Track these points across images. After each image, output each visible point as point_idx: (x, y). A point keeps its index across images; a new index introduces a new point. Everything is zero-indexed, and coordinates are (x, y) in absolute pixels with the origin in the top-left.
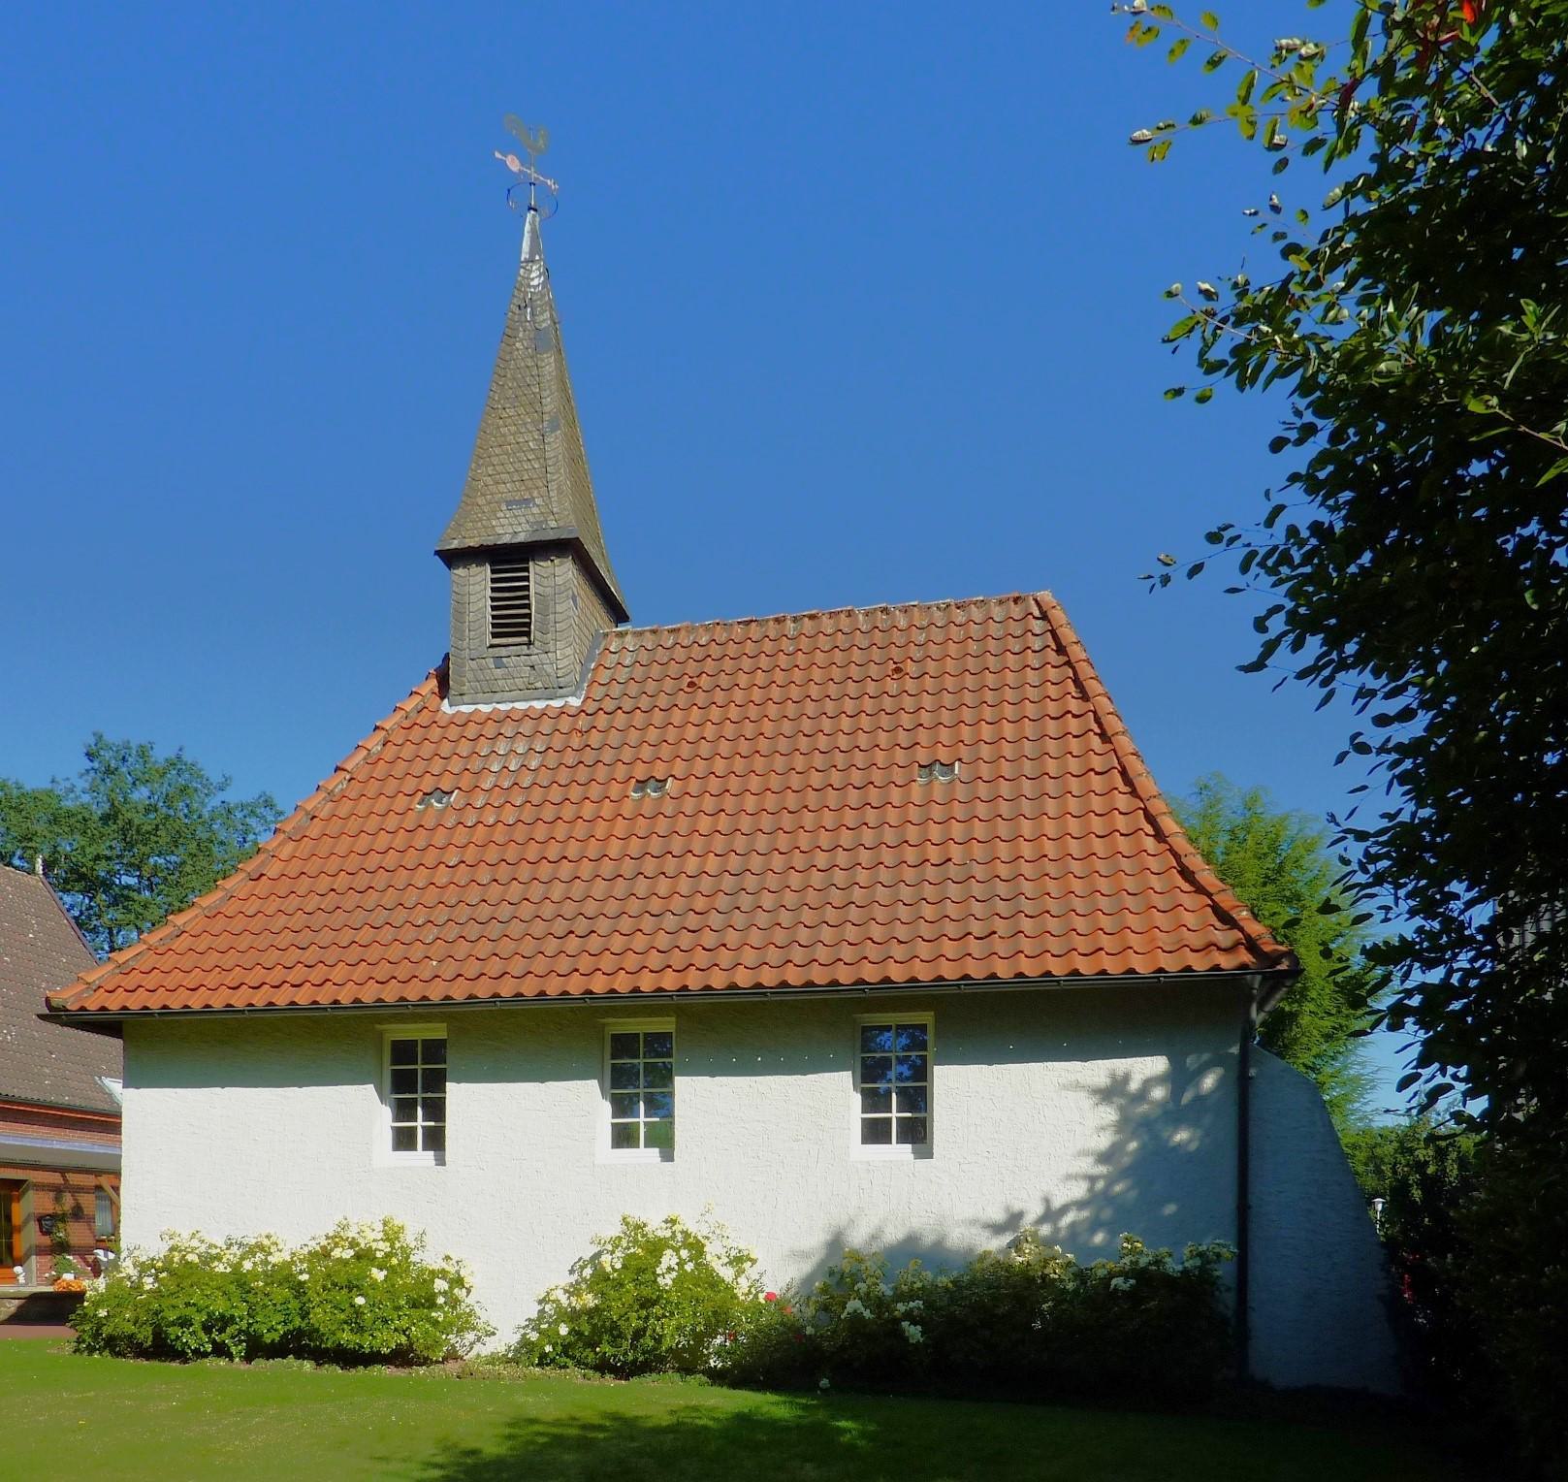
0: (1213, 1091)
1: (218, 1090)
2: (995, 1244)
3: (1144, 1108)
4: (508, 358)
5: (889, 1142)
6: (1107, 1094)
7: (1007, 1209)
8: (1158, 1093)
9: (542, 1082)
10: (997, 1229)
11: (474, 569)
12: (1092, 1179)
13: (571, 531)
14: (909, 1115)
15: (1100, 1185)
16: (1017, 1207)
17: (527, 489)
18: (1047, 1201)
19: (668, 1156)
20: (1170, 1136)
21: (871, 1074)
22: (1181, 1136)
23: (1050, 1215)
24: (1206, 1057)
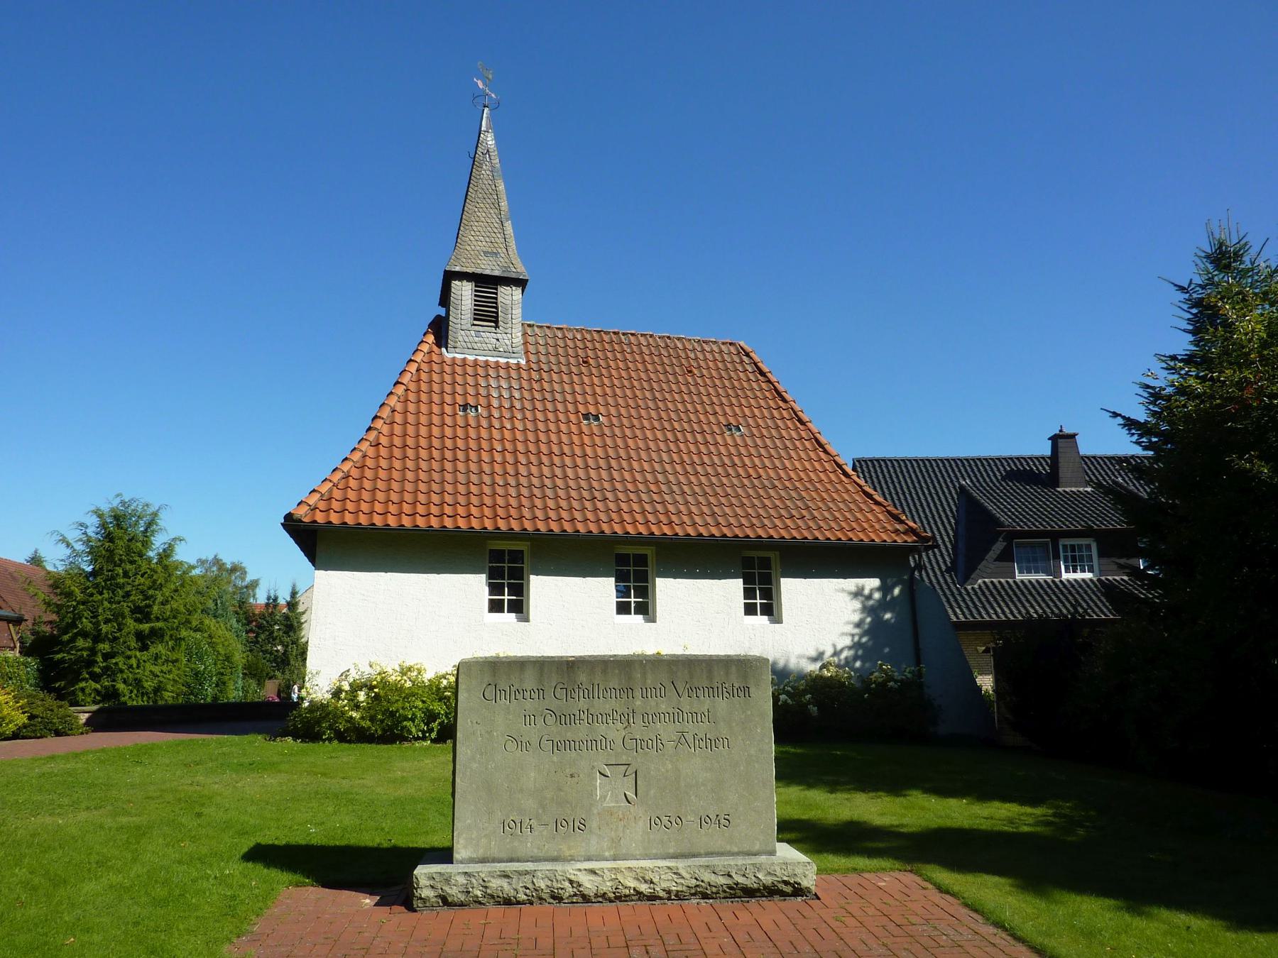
0: (899, 596)
1: (383, 574)
2: (813, 668)
3: (871, 602)
4: (478, 177)
5: (630, 614)
6: (857, 594)
7: (817, 650)
8: (877, 596)
9: (584, 577)
10: (814, 660)
11: (465, 283)
12: (853, 635)
13: (524, 276)
14: (515, 598)
15: (856, 638)
16: (821, 649)
17: (495, 247)
18: (834, 646)
19: (778, 620)
20: (883, 616)
21: (620, 577)
22: (888, 616)
23: (836, 653)
24: (895, 580)
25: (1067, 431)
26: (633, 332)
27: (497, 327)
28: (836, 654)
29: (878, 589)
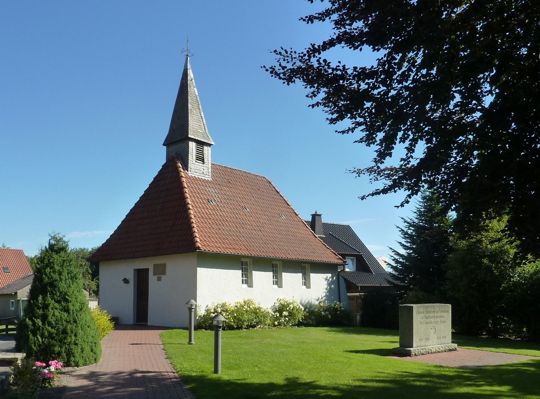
25: (318, 213)
26: (236, 169)
27: (203, 163)
28: (322, 298)
29: (331, 277)
